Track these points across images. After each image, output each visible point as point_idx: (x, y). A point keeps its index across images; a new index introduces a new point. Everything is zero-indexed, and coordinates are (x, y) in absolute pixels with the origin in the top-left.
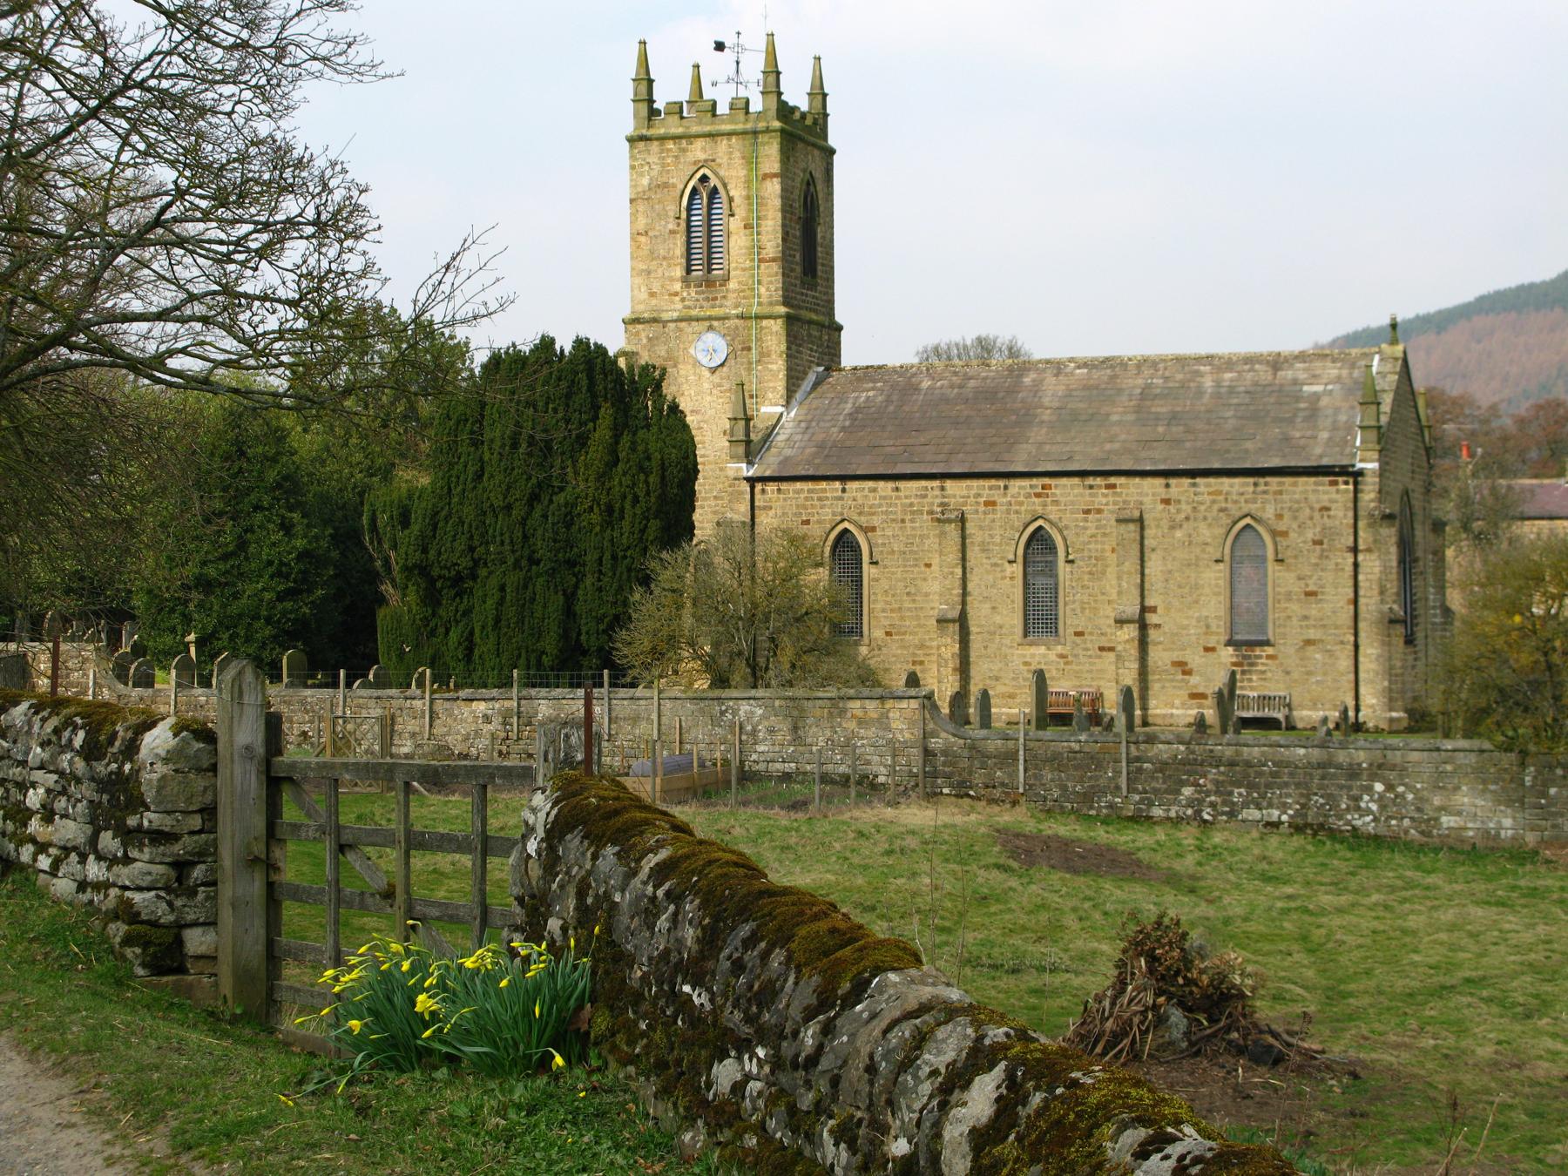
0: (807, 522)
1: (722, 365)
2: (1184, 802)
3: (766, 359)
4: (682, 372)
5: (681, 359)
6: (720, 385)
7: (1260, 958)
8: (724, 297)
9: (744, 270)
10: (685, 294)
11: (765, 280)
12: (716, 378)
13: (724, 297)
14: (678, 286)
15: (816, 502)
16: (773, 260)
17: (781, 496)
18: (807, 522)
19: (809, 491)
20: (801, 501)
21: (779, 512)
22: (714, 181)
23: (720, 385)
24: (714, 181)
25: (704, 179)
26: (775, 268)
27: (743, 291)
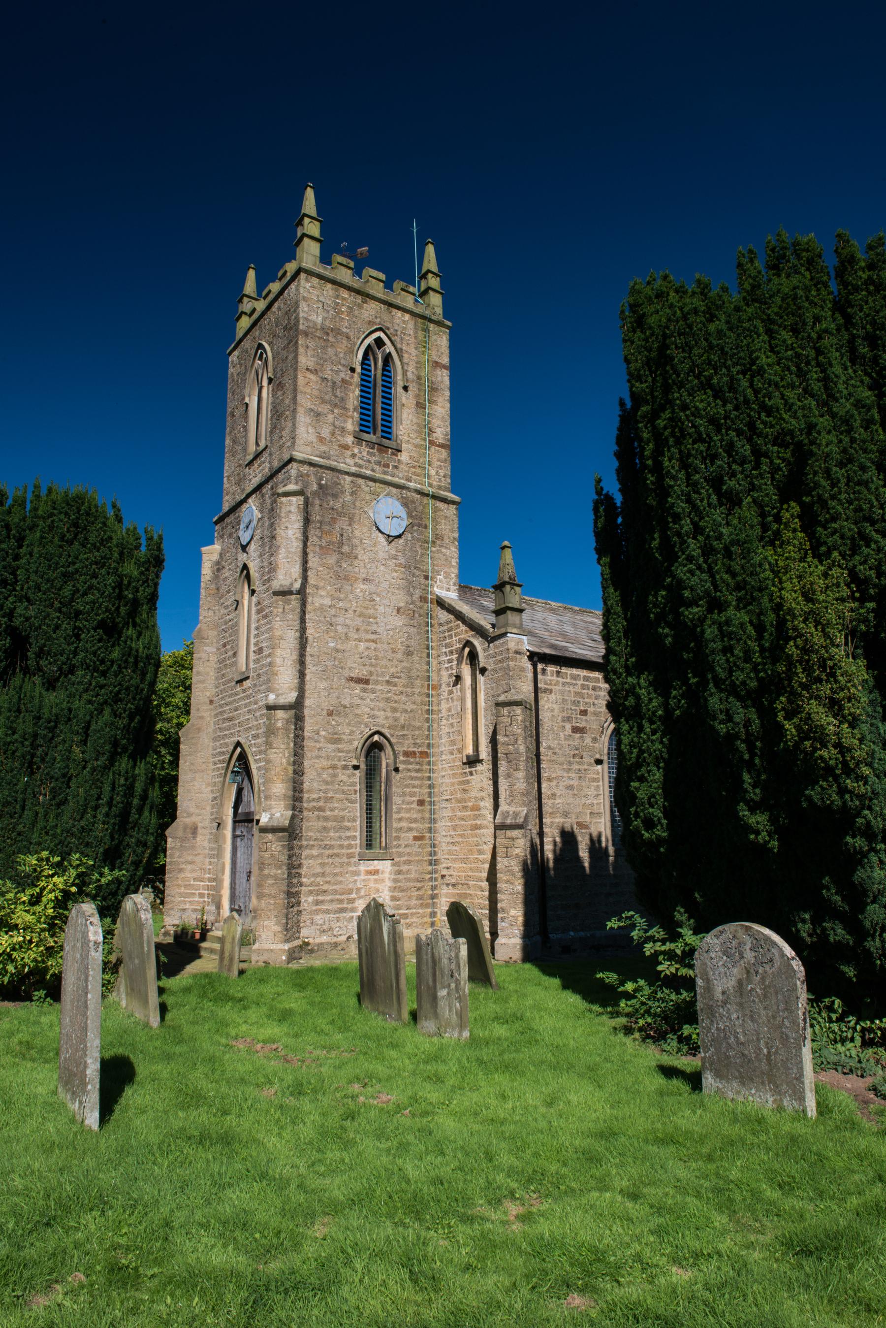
0: (584, 713)
1: (399, 536)
2: (661, 958)
3: (438, 542)
4: (356, 533)
5: (356, 518)
6: (395, 557)
7: (338, 897)
8: (396, 467)
9: (416, 446)
10: (356, 451)
11: (436, 463)
12: (392, 549)
13: (396, 467)
14: (349, 440)
15: (591, 692)
16: (442, 446)
17: (560, 679)
18: (584, 713)
19: (586, 679)
20: (578, 689)
21: (560, 697)
22: (389, 348)
23: (395, 557)
24: (389, 348)
25: (379, 342)
26: (444, 454)
27: (414, 467)
